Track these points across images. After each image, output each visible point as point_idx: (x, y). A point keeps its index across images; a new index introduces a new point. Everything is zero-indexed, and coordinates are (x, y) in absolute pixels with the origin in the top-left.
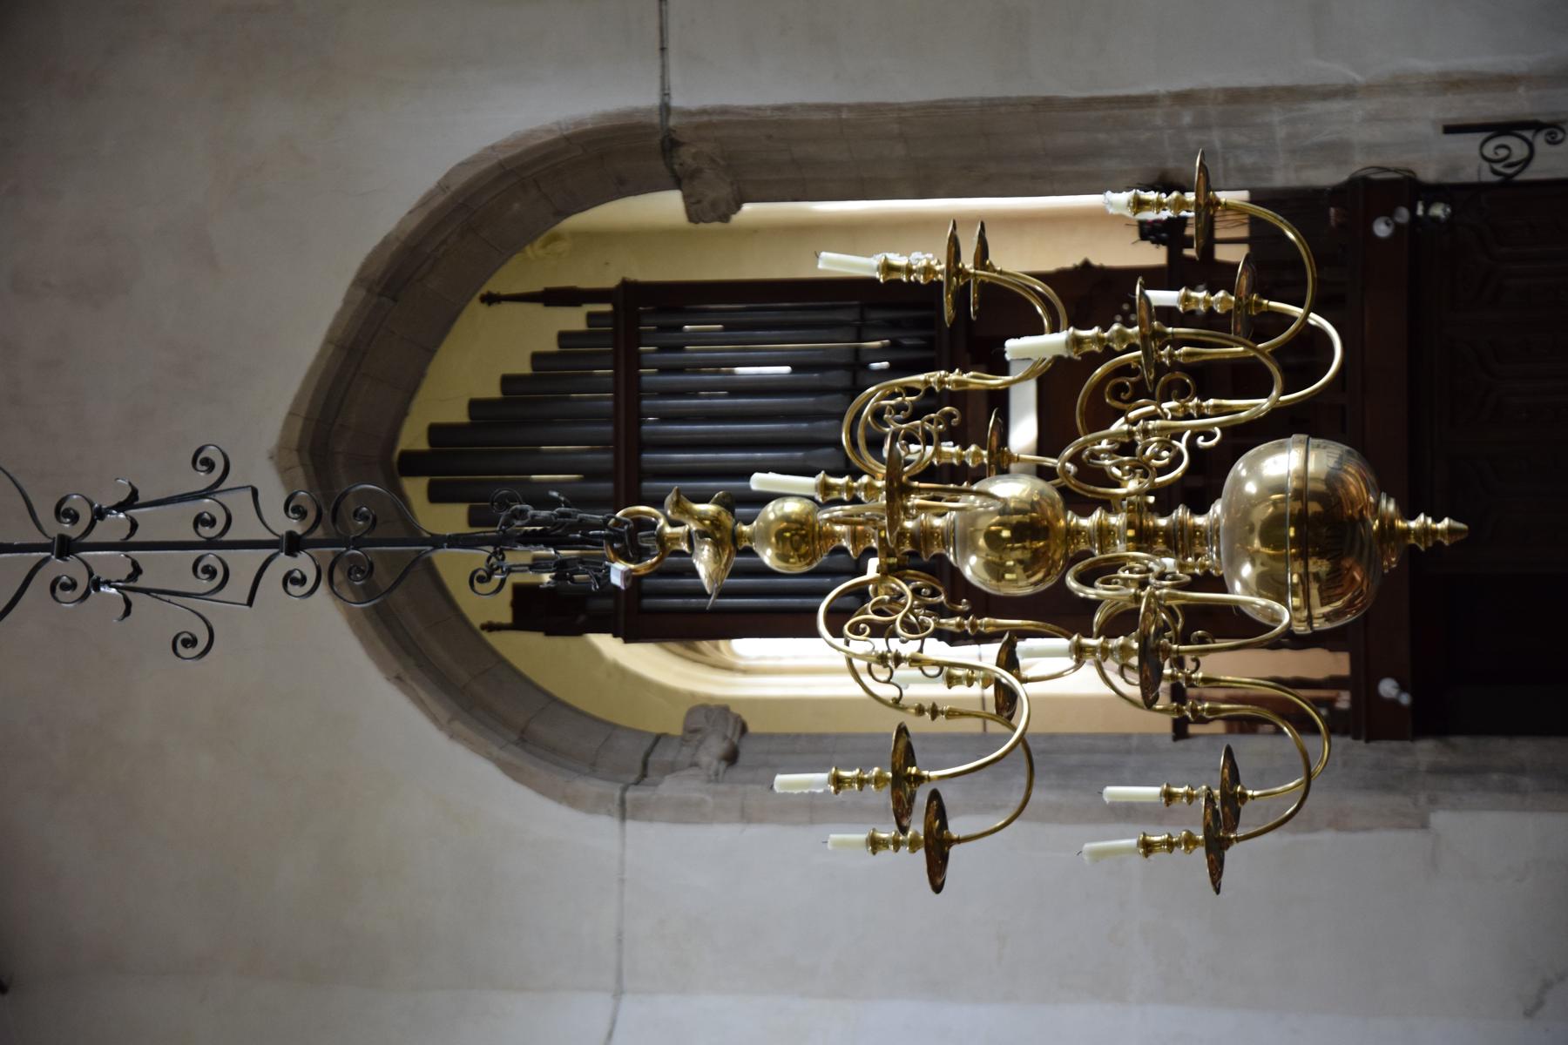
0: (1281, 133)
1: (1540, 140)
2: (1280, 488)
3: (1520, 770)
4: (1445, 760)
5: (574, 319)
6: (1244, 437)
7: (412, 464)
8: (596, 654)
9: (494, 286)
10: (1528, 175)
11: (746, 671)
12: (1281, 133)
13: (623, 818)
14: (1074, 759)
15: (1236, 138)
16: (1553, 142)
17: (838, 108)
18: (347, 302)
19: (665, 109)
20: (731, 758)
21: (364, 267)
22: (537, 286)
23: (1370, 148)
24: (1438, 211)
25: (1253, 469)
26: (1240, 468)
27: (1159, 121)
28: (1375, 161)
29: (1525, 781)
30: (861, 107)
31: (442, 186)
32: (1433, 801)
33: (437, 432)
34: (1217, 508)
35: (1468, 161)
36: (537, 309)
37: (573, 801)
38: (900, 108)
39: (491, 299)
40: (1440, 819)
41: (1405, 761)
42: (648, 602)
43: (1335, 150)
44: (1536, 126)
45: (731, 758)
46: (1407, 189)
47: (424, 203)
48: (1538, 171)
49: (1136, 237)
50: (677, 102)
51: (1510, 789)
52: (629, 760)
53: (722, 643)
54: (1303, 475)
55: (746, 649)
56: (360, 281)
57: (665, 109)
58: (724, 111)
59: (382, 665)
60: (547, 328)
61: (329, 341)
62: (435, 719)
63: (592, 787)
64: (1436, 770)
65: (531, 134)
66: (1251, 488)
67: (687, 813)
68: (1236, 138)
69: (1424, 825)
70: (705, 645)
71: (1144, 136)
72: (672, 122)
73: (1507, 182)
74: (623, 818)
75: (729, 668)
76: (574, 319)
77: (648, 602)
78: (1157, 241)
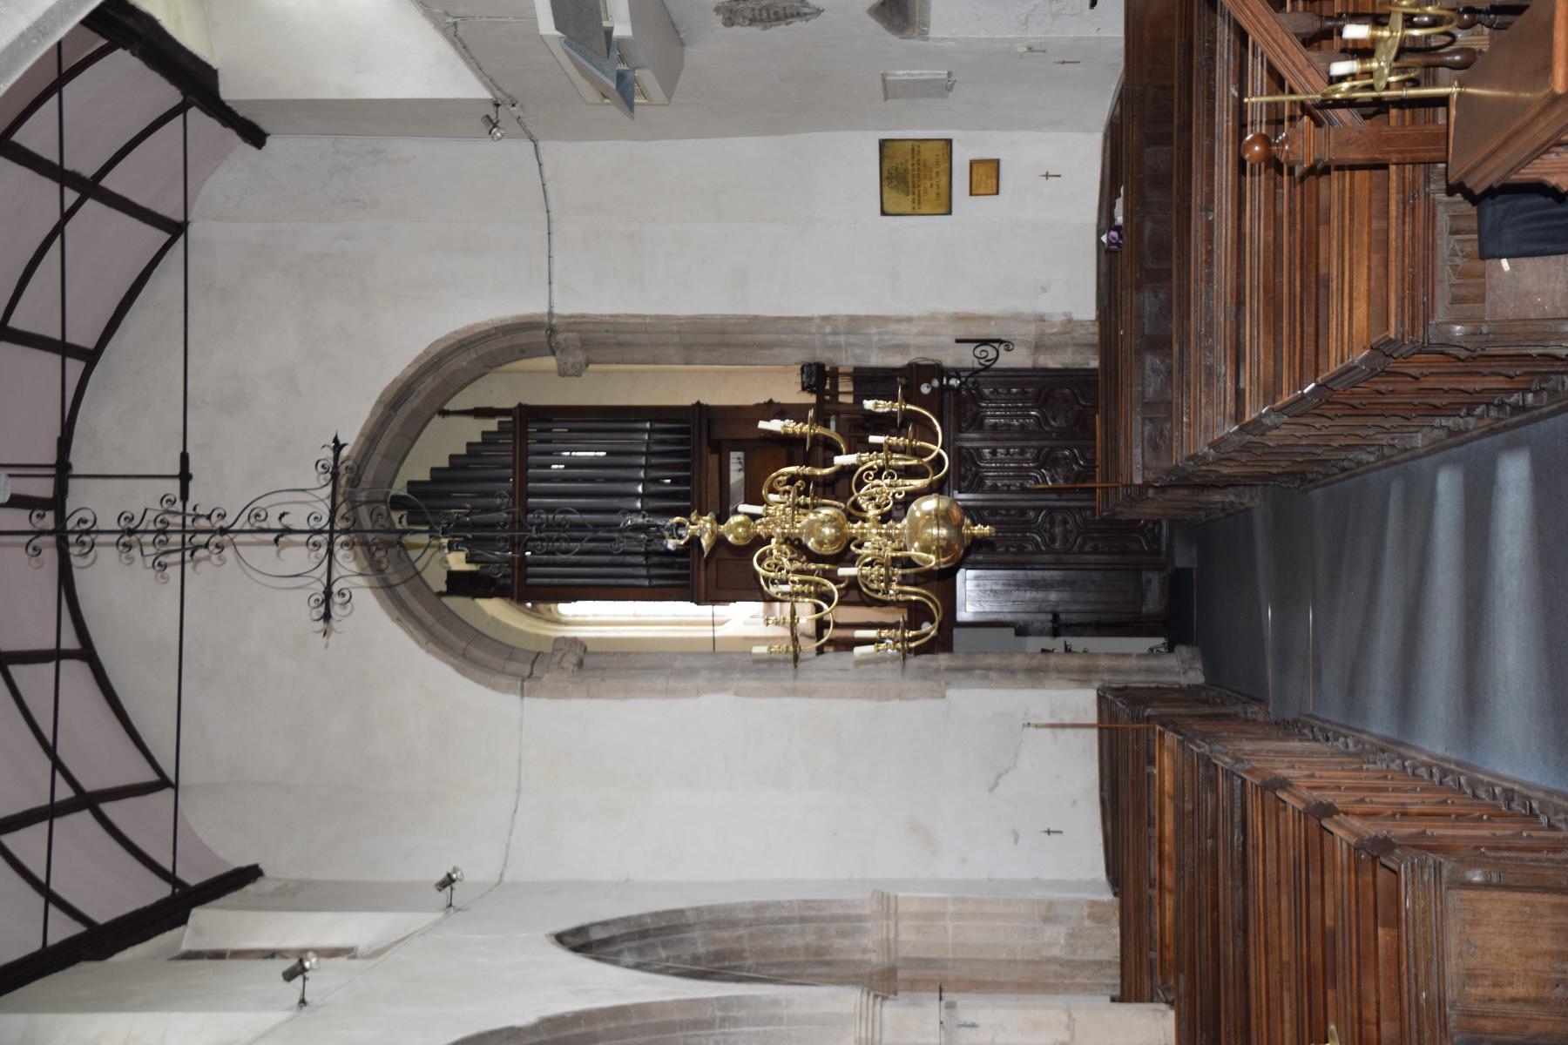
0: (875, 339)
1: (1002, 349)
2: (929, 513)
3: (989, 668)
4: (954, 664)
5: (492, 425)
6: (913, 496)
7: (397, 503)
8: (482, 612)
9: (449, 407)
10: (996, 366)
11: (566, 624)
12: (875, 339)
13: (522, 696)
14: (1420, 297)
15: (852, 339)
16: (1008, 350)
17: (645, 317)
18: (372, 414)
19: (551, 314)
20: (580, 664)
21: (382, 395)
22: (471, 407)
23: (920, 348)
24: (954, 382)
25: (918, 506)
26: (913, 506)
27: (813, 330)
28: (921, 355)
29: (992, 674)
30: (658, 317)
31: (426, 352)
32: (947, 684)
33: (411, 484)
34: (905, 521)
35: (966, 357)
36: (470, 420)
37: (495, 687)
38: (678, 318)
39: (444, 413)
40: (951, 693)
41: (933, 664)
42: (530, 581)
43: (902, 348)
44: (1000, 342)
45: (580, 664)
46: (937, 370)
47: (415, 361)
48: (999, 364)
49: (799, 388)
50: (556, 311)
51: (985, 677)
52: (529, 667)
53: (552, 606)
54: (937, 510)
55: (565, 609)
56: (379, 402)
57: (551, 314)
58: (583, 316)
59: (388, 611)
60: (474, 430)
61: (361, 434)
62: (418, 642)
63: (505, 681)
64: (949, 669)
65: (477, 325)
66: (918, 514)
67: (557, 693)
68: (852, 339)
69: (944, 696)
70: (541, 607)
71: (805, 337)
72: (554, 321)
73: (987, 368)
74: (522, 696)
75: (558, 622)
76: (492, 425)
77: (530, 581)
78: (812, 392)
